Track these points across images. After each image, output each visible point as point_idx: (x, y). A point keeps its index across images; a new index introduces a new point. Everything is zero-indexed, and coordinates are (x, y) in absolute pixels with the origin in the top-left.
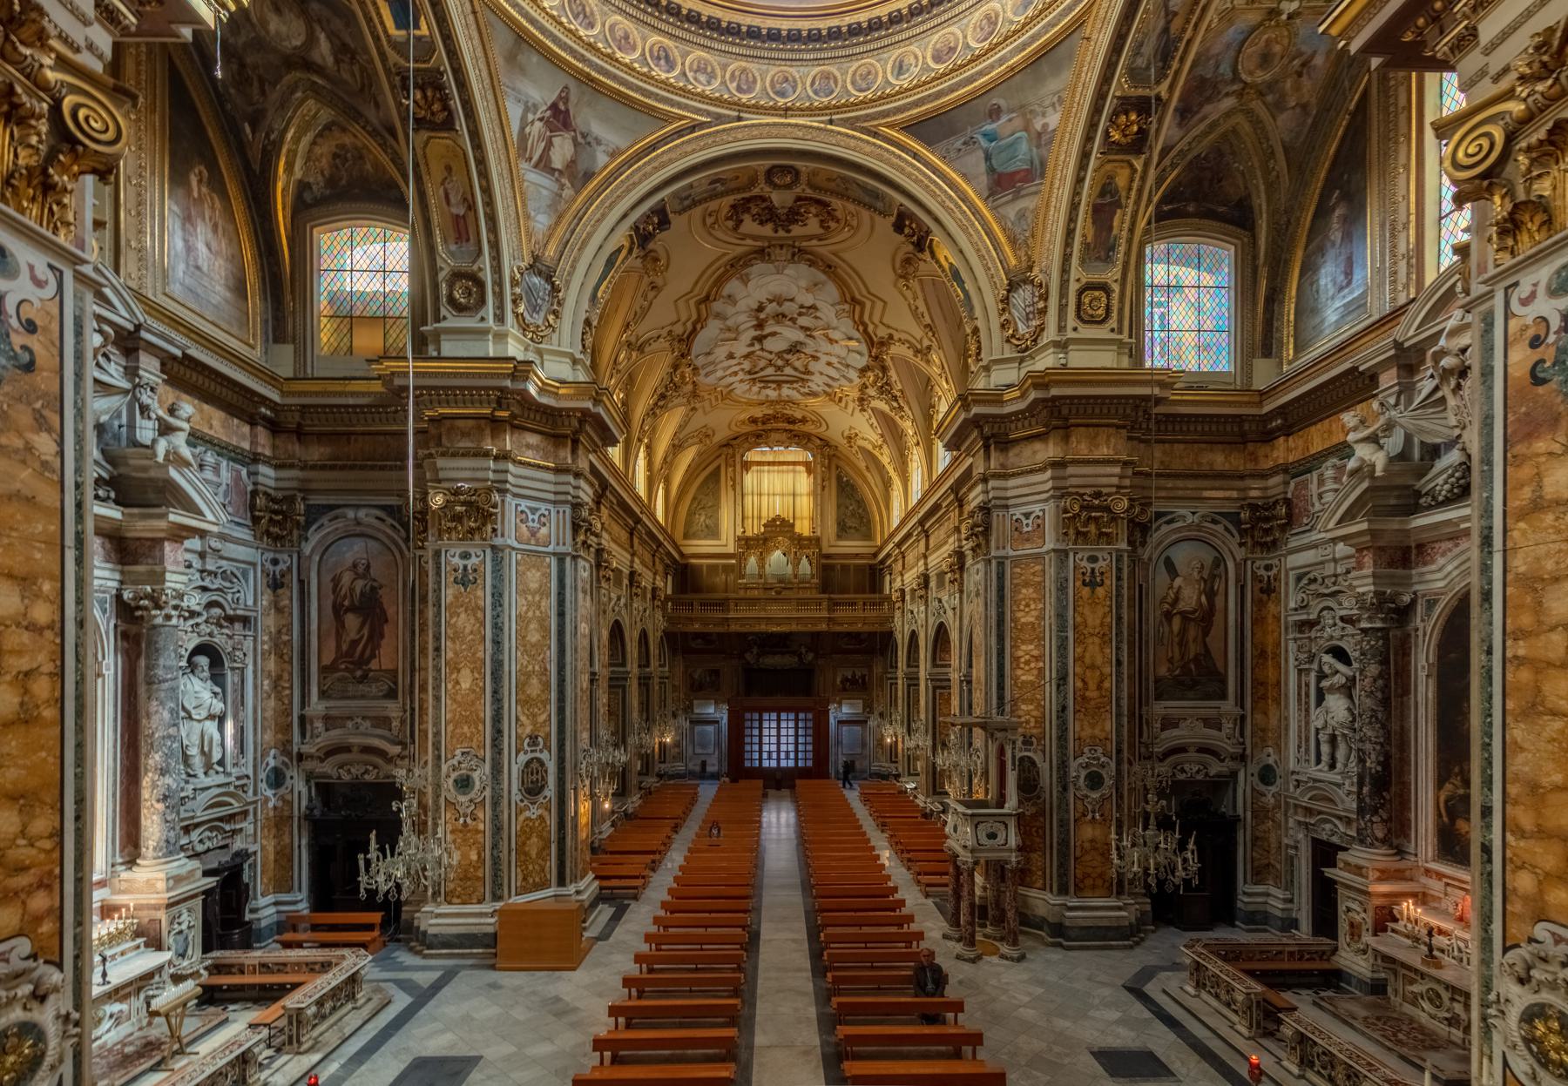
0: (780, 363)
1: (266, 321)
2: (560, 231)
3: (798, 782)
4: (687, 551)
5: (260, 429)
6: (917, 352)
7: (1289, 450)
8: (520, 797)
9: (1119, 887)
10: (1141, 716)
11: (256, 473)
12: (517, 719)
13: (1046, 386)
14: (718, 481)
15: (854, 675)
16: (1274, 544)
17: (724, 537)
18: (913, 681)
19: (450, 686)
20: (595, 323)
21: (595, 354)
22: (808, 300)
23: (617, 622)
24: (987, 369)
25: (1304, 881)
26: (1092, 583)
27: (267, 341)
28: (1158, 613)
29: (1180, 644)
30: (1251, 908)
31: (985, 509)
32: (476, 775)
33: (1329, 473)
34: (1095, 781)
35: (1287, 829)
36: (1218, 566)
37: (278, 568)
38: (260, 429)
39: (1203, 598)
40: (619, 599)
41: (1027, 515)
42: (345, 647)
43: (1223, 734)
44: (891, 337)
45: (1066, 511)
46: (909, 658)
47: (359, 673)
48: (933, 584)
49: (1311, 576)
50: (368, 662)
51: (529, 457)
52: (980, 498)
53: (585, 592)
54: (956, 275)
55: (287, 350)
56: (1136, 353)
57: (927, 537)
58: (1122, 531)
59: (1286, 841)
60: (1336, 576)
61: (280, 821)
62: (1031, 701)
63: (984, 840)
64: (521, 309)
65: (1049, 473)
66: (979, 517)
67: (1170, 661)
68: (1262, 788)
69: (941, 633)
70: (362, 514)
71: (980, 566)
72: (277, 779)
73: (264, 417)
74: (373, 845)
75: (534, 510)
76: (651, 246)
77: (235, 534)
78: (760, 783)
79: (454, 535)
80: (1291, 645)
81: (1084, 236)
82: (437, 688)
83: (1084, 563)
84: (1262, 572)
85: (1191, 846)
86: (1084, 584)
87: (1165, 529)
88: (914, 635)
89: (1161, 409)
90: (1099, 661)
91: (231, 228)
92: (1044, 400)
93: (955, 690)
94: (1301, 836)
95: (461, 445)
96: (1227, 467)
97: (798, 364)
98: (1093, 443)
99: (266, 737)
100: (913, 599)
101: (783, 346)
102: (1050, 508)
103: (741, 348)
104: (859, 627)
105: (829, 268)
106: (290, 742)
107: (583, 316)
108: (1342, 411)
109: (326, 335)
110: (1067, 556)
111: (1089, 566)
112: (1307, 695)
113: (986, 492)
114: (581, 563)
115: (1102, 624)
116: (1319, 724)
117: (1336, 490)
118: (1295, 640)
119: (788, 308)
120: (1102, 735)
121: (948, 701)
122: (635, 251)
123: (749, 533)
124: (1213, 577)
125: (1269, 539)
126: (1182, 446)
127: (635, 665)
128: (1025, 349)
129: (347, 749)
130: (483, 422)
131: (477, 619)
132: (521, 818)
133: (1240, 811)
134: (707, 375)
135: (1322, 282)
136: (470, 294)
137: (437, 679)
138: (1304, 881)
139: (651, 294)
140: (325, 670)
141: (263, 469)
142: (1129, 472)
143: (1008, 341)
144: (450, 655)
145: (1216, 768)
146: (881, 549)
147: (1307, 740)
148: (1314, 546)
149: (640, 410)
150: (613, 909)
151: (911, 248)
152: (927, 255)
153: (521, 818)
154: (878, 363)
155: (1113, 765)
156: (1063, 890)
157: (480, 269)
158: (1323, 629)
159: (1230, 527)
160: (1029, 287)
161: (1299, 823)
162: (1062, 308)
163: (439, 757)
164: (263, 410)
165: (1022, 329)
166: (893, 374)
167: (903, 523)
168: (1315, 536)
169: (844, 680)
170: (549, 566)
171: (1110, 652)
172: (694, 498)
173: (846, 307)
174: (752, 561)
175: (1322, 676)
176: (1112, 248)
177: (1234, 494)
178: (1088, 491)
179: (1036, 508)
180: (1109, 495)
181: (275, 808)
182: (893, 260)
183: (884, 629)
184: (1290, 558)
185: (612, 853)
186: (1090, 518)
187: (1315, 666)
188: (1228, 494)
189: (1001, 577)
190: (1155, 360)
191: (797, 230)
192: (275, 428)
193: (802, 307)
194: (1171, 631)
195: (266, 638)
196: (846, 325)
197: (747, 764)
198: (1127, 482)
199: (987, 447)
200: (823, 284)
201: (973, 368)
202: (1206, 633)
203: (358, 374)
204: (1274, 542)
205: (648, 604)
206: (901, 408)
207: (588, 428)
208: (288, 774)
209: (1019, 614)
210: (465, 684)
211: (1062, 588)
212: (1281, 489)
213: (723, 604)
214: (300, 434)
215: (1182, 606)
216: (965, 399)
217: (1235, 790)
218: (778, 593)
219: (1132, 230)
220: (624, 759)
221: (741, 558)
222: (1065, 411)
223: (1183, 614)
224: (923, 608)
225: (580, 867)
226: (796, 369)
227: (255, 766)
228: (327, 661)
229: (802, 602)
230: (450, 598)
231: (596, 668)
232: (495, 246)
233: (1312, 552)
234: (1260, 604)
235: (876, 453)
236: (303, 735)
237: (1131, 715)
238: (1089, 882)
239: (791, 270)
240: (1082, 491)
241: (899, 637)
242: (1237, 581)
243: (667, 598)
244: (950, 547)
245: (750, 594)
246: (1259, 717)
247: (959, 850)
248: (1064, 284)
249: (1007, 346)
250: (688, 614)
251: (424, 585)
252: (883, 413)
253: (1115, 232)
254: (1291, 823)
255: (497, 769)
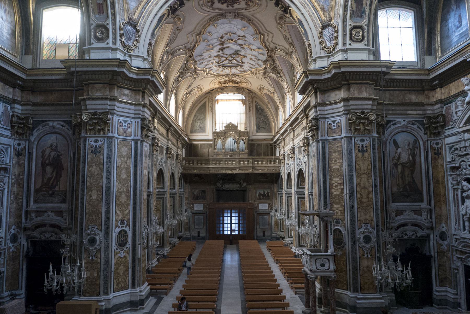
0: (230, 59)
1: (22, 46)
2: (140, 8)
3: (240, 241)
4: (192, 138)
5: (17, 89)
6: (287, 54)
7: (442, 94)
8: (116, 247)
9: (379, 289)
10: (386, 210)
11: (14, 108)
12: (116, 212)
13: (339, 67)
14: (205, 108)
15: (264, 192)
16: (439, 134)
17: (207, 131)
18: (289, 195)
19: (88, 198)
20: (153, 44)
21: (153, 56)
22: (242, 33)
23: (161, 169)
24: (315, 60)
25: (462, 285)
26: (362, 150)
27: (22, 54)
28: (392, 164)
29: (402, 177)
30: (439, 298)
31: (316, 119)
32: (97, 238)
33: (459, 103)
34: (367, 239)
35: (453, 261)
36: (416, 143)
37: (20, 147)
38: (17, 89)
39: (411, 157)
40: (162, 159)
41: (334, 122)
42: (45, 181)
43: (422, 218)
44: (276, 48)
45: (350, 120)
46: (287, 185)
47: (50, 192)
48: (296, 152)
49: (455, 147)
50: (54, 188)
51: (124, 99)
52: (314, 115)
53: (146, 157)
54: (301, 23)
55: (30, 57)
56: (376, 53)
57: (294, 131)
58: (374, 128)
59: (453, 266)
60: (466, 147)
61: (14, 258)
62: (339, 203)
63: (319, 267)
64: (123, 40)
65: (342, 104)
66: (314, 122)
67: (398, 185)
68: (441, 242)
69: (301, 173)
70: (55, 124)
71: (315, 144)
72: (14, 239)
73: (19, 85)
74: (51, 269)
75: (125, 122)
76: (177, 13)
77: (4, 133)
78: (223, 242)
79: (92, 132)
80: (449, 177)
81: (351, 7)
82: (82, 199)
83: (359, 142)
84: (435, 146)
85: (409, 268)
86: (359, 151)
87: (393, 127)
88: (289, 174)
89: (387, 77)
90: (367, 185)
91: (11, 11)
92: (338, 73)
93: (307, 199)
94: (459, 264)
95: (97, 95)
96: (417, 101)
97: (238, 59)
98: (360, 91)
99: (11, 220)
100: (288, 158)
101: (232, 52)
102: (343, 118)
103: (214, 53)
104: (266, 171)
105: (250, 20)
106: (21, 222)
107: (148, 41)
108: (462, 77)
109: (46, 52)
110: (351, 139)
111: (361, 143)
112: (458, 200)
113: (316, 112)
114: (145, 144)
115: (367, 169)
116: (463, 212)
117: (462, 110)
118: (451, 175)
119: (235, 37)
120: (370, 219)
121: (304, 204)
122: (170, 15)
123: (218, 130)
124: (414, 148)
125: (437, 131)
126: (397, 92)
127: (169, 188)
128: (330, 53)
129: (44, 225)
130: (105, 85)
131: (100, 168)
132: (116, 257)
133: (432, 253)
134: (200, 64)
135: (450, 25)
136: (103, 34)
137: (83, 195)
138: (462, 285)
139: (177, 32)
140: (37, 191)
141: (17, 106)
142: (376, 103)
143: (323, 49)
144: (88, 184)
145: (421, 233)
146: (275, 136)
147: (459, 220)
148: (456, 134)
149: (172, 80)
150: (156, 300)
151: (282, 13)
152: (288, 15)
153: (116, 257)
154: (271, 58)
155: (375, 232)
156: (355, 290)
157: (108, 24)
158: (462, 170)
159: (420, 126)
160: (330, 28)
161: (458, 258)
162: (344, 36)
163: (82, 229)
164: (18, 82)
165: (328, 44)
166: (277, 62)
167: (283, 125)
168: (455, 130)
169: (260, 195)
170: (131, 145)
171: (372, 181)
172: (195, 116)
173: (257, 36)
174: (220, 142)
175: (463, 191)
176: (363, 12)
177: (421, 112)
178: (359, 111)
179: (338, 119)
180: (368, 113)
181: (13, 252)
182: (276, 18)
183: (277, 171)
184: (446, 139)
185: (156, 273)
186: (360, 122)
187: (460, 187)
188: (418, 112)
189: (324, 148)
190: (384, 56)
191: (236, 6)
192: (23, 89)
193: (239, 36)
194: (398, 171)
195: (13, 177)
196: (258, 43)
197: (218, 233)
198: (375, 107)
199: (316, 93)
200: (248, 27)
201: (310, 61)
202: (413, 172)
203: (56, 67)
204: (439, 133)
205: (175, 161)
206: (281, 77)
207: (149, 87)
208: (19, 236)
209: (332, 165)
210: (94, 197)
211: (350, 153)
212: (440, 110)
213: (207, 160)
214: (33, 91)
215: (402, 161)
216: (306, 73)
217: (429, 243)
218: (231, 156)
219: (371, 5)
220: (162, 230)
221: (215, 141)
222: (348, 78)
223: (402, 164)
224: (293, 162)
225: (142, 279)
226: (237, 61)
227: (5, 233)
228: (38, 187)
229: (241, 160)
230: (89, 159)
231: (151, 190)
232: (114, 14)
233: (455, 137)
234: (434, 160)
235: (272, 95)
236: (26, 219)
237: (382, 209)
238: (366, 286)
239: (234, 22)
240: (356, 111)
241: (283, 175)
242: (425, 149)
243: (183, 159)
244: (302, 136)
245: (219, 157)
246: (438, 210)
247: (309, 272)
248: (344, 26)
249: (322, 51)
250: (192, 165)
251: (79, 154)
252: (274, 79)
253: (364, 6)
254: (455, 258)
255: (107, 233)
